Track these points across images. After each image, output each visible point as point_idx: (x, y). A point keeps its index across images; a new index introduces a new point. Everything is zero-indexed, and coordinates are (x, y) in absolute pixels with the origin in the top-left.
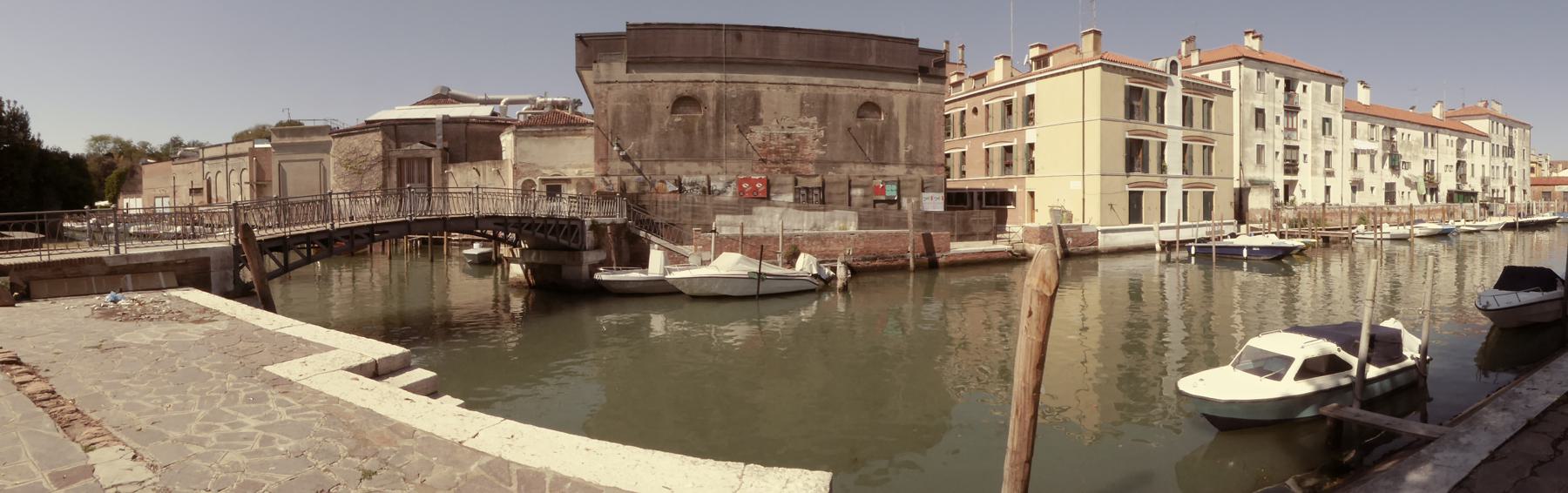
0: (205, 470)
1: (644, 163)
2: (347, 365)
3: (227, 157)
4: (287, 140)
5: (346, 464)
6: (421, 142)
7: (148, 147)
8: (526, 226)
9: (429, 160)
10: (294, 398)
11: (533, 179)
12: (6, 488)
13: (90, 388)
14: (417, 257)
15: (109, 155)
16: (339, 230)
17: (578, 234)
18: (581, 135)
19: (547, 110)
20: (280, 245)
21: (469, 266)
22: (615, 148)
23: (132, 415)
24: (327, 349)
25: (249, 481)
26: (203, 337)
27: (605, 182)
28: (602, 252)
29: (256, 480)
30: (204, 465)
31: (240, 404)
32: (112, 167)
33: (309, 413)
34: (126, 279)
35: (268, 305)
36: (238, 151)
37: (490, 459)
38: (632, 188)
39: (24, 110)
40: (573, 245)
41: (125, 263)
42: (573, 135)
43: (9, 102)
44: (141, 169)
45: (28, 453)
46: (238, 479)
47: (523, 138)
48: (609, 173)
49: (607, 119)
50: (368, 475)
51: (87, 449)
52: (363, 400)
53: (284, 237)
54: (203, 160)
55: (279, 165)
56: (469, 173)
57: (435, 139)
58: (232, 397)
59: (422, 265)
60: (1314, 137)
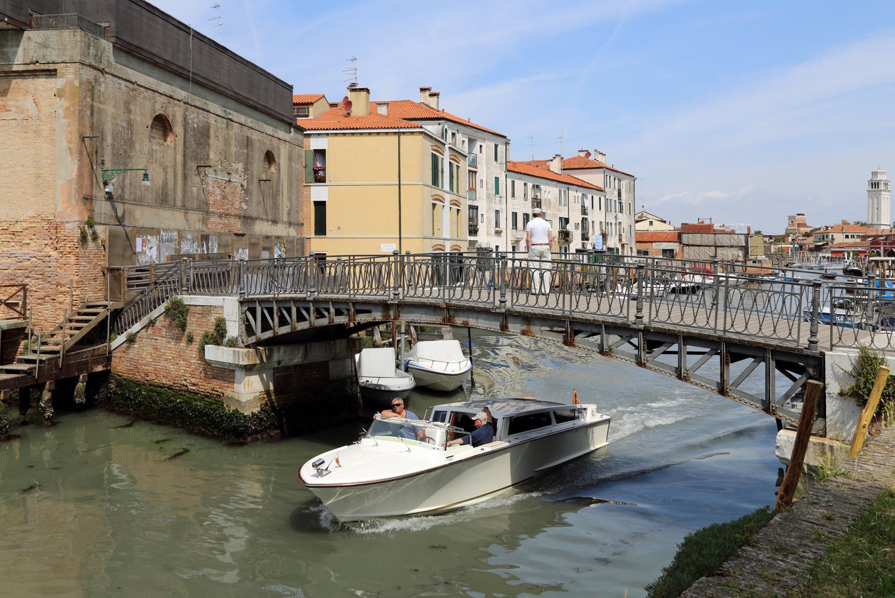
60: (488, 197)
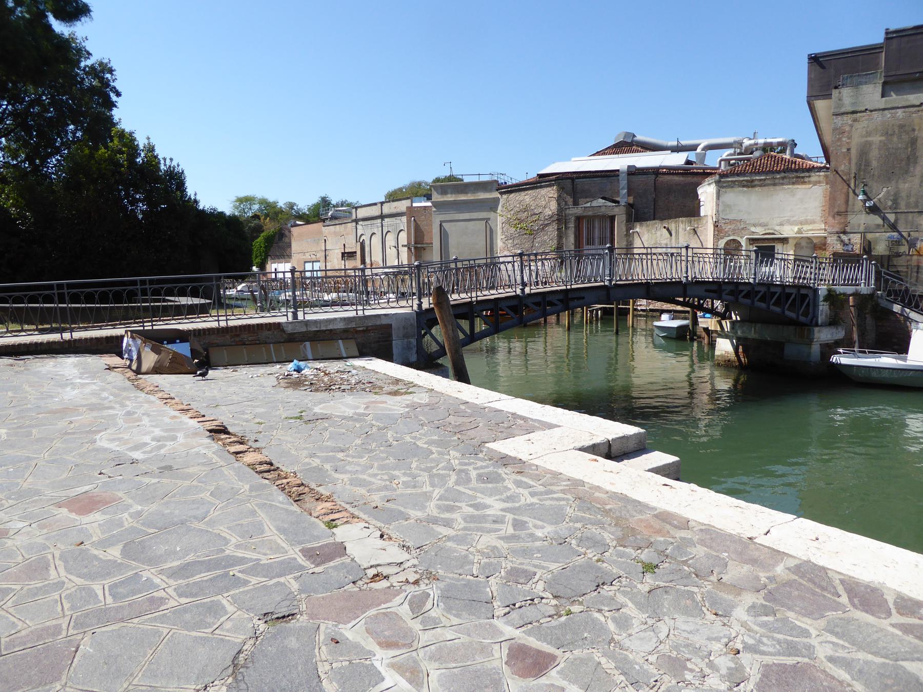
0: (463, 554)
1: (902, 217)
2: (579, 445)
3: (382, 217)
4: (450, 198)
5: (621, 555)
6: (603, 198)
7: (295, 207)
8: (743, 294)
9: (612, 218)
10: (532, 479)
11: (739, 239)
12: (262, 562)
13: (307, 460)
14: (597, 331)
15: (256, 217)
16: (530, 295)
17: (808, 304)
18: (804, 183)
19: (757, 154)
20: (468, 311)
21: (663, 342)
22: (861, 197)
23: (362, 491)
24: (551, 426)
25: (515, 568)
26: (407, 410)
27: (842, 241)
28: (840, 329)
29: (525, 567)
30: (462, 549)
31: (474, 483)
32: (259, 229)
33: (555, 496)
34: (305, 346)
35: (462, 376)
36: (393, 211)
37: (797, 562)
38: (881, 249)
39: (180, 168)
40: (802, 319)
41: (304, 329)
42: (793, 184)
43: (165, 159)
44: (290, 232)
45: (271, 527)
46: (504, 565)
47: (729, 189)
48: (848, 229)
49: (850, 159)
50: (649, 568)
51: (331, 525)
52: (612, 484)
53: (471, 302)
54: (356, 221)
55: (441, 225)
56: (659, 233)
57: (618, 193)
58: (463, 475)
59: (605, 339)
